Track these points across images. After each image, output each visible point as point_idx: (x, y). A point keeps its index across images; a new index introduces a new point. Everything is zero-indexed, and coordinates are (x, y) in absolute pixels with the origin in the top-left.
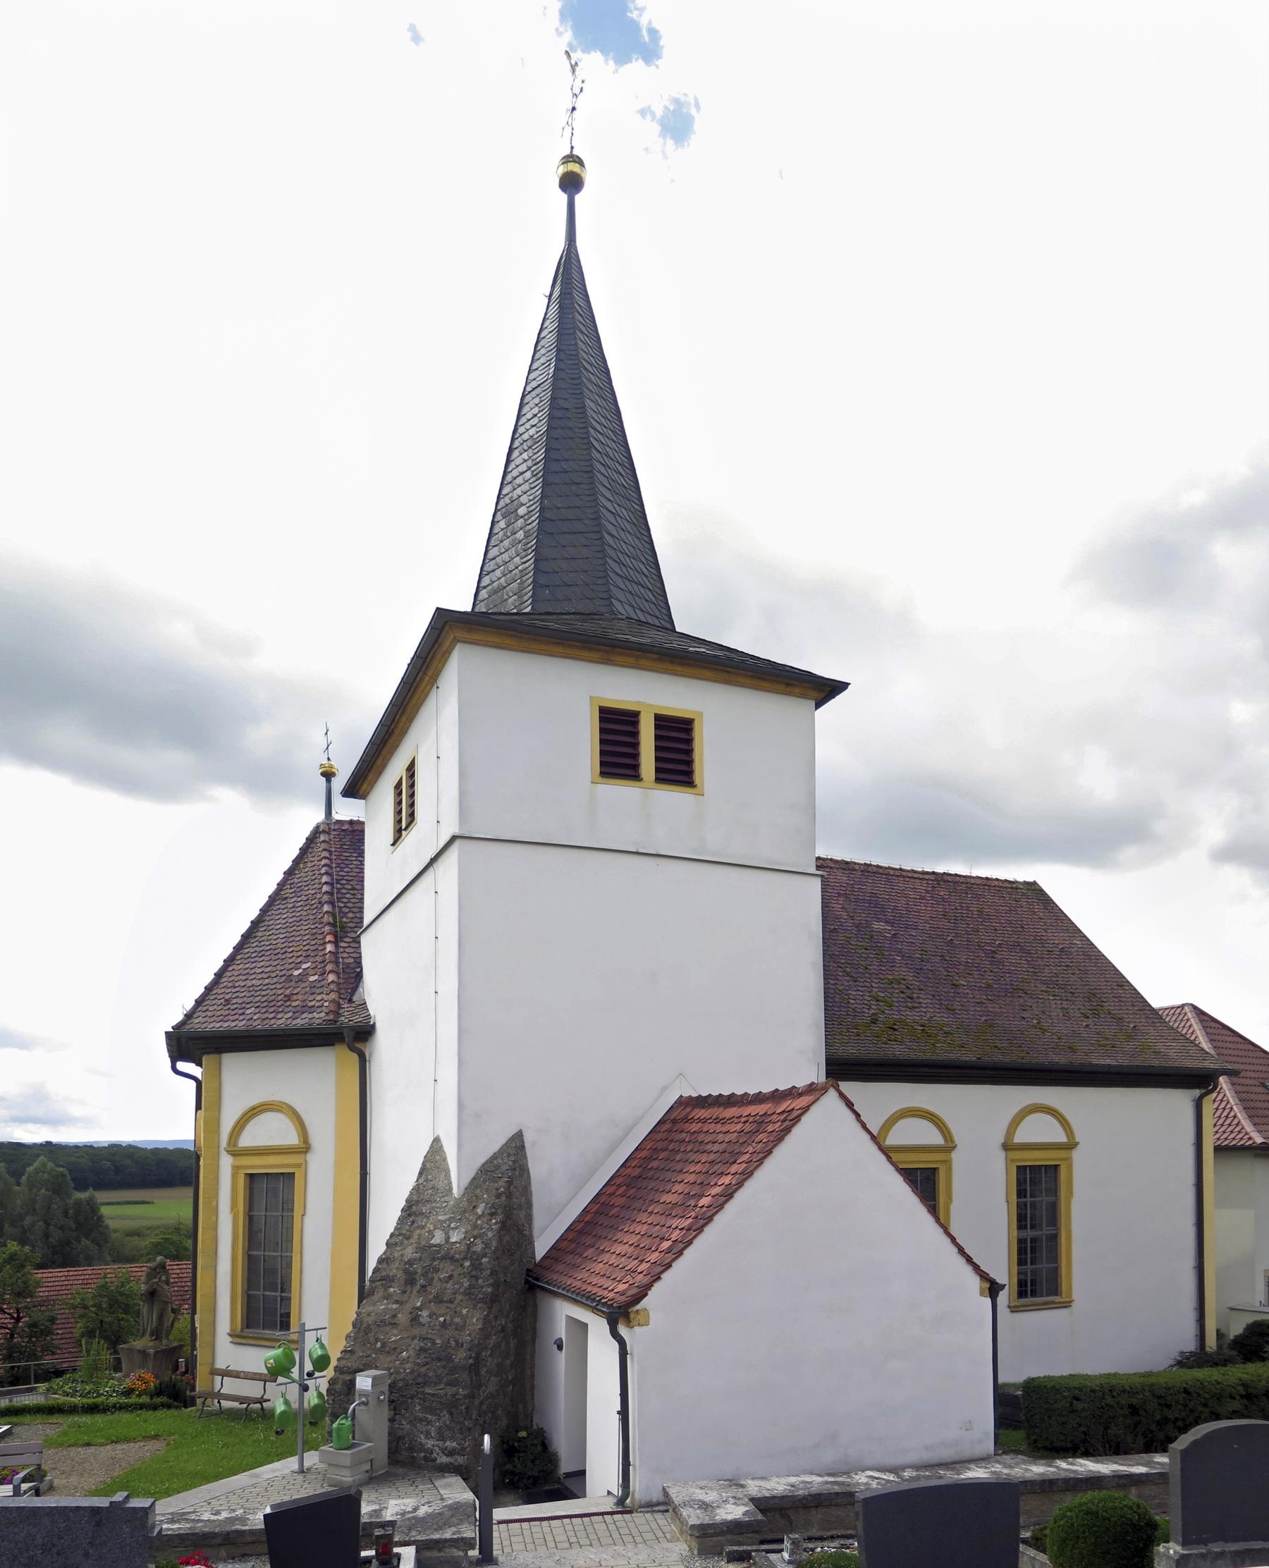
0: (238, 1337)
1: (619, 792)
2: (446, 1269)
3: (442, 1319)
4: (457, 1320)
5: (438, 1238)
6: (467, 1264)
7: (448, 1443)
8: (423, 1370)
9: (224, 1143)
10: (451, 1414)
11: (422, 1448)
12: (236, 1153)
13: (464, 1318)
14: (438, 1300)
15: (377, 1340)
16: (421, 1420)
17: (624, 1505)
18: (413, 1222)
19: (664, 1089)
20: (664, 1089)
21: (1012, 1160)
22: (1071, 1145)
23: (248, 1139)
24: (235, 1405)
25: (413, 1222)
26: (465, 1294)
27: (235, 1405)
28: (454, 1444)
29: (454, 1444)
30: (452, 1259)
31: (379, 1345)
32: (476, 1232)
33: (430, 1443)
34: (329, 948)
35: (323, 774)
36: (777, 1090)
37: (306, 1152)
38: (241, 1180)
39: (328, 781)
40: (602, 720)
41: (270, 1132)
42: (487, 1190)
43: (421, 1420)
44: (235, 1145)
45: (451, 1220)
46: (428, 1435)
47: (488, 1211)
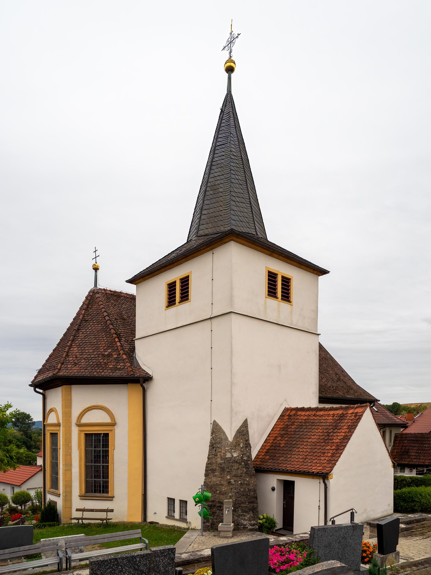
0: (83, 497)
1: (272, 302)
2: (236, 466)
3: (240, 482)
4: (246, 482)
5: (228, 455)
6: (243, 464)
7: (252, 522)
8: (240, 499)
9: (74, 420)
10: (253, 512)
11: (242, 524)
12: (79, 425)
13: (248, 481)
14: (236, 476)
15: (217, 490)
16: (242, 515)
17: (67, 569)
18: (216, 450)
19: (281, 404)
20: (281, 404)
21: (81, 431)
22: (113, 424)
23: (85, 420)
24: (99, 521)
25: (216, 450)
26: (245, 473)
27: (99, 521)
28: (255, 522)
29: (255, 522)
30: (237, 462)
31: (218, 492)
32: (242, 453)
33: (245, 523)
34: (119, 344)
35: (94, 269)
36: (297, 407)
37: (114, 425)
38: (83, 437)
39: (96, 272)
40: (269, 276)
41: (96, 417)
42: (241, 439)
43: (242, 515)
44: (80, 422)
45: (231, 449)
46: (245, 520)
47: (244, 446)
